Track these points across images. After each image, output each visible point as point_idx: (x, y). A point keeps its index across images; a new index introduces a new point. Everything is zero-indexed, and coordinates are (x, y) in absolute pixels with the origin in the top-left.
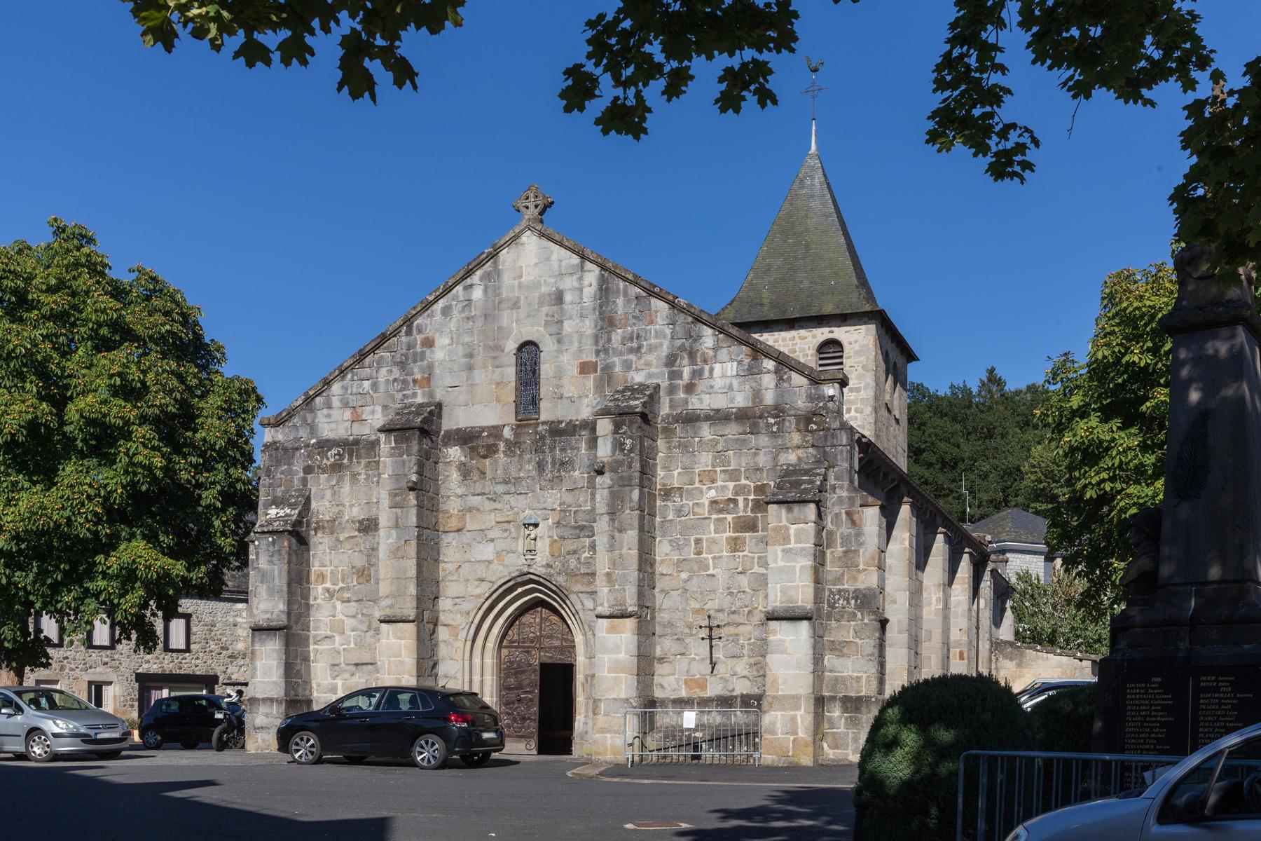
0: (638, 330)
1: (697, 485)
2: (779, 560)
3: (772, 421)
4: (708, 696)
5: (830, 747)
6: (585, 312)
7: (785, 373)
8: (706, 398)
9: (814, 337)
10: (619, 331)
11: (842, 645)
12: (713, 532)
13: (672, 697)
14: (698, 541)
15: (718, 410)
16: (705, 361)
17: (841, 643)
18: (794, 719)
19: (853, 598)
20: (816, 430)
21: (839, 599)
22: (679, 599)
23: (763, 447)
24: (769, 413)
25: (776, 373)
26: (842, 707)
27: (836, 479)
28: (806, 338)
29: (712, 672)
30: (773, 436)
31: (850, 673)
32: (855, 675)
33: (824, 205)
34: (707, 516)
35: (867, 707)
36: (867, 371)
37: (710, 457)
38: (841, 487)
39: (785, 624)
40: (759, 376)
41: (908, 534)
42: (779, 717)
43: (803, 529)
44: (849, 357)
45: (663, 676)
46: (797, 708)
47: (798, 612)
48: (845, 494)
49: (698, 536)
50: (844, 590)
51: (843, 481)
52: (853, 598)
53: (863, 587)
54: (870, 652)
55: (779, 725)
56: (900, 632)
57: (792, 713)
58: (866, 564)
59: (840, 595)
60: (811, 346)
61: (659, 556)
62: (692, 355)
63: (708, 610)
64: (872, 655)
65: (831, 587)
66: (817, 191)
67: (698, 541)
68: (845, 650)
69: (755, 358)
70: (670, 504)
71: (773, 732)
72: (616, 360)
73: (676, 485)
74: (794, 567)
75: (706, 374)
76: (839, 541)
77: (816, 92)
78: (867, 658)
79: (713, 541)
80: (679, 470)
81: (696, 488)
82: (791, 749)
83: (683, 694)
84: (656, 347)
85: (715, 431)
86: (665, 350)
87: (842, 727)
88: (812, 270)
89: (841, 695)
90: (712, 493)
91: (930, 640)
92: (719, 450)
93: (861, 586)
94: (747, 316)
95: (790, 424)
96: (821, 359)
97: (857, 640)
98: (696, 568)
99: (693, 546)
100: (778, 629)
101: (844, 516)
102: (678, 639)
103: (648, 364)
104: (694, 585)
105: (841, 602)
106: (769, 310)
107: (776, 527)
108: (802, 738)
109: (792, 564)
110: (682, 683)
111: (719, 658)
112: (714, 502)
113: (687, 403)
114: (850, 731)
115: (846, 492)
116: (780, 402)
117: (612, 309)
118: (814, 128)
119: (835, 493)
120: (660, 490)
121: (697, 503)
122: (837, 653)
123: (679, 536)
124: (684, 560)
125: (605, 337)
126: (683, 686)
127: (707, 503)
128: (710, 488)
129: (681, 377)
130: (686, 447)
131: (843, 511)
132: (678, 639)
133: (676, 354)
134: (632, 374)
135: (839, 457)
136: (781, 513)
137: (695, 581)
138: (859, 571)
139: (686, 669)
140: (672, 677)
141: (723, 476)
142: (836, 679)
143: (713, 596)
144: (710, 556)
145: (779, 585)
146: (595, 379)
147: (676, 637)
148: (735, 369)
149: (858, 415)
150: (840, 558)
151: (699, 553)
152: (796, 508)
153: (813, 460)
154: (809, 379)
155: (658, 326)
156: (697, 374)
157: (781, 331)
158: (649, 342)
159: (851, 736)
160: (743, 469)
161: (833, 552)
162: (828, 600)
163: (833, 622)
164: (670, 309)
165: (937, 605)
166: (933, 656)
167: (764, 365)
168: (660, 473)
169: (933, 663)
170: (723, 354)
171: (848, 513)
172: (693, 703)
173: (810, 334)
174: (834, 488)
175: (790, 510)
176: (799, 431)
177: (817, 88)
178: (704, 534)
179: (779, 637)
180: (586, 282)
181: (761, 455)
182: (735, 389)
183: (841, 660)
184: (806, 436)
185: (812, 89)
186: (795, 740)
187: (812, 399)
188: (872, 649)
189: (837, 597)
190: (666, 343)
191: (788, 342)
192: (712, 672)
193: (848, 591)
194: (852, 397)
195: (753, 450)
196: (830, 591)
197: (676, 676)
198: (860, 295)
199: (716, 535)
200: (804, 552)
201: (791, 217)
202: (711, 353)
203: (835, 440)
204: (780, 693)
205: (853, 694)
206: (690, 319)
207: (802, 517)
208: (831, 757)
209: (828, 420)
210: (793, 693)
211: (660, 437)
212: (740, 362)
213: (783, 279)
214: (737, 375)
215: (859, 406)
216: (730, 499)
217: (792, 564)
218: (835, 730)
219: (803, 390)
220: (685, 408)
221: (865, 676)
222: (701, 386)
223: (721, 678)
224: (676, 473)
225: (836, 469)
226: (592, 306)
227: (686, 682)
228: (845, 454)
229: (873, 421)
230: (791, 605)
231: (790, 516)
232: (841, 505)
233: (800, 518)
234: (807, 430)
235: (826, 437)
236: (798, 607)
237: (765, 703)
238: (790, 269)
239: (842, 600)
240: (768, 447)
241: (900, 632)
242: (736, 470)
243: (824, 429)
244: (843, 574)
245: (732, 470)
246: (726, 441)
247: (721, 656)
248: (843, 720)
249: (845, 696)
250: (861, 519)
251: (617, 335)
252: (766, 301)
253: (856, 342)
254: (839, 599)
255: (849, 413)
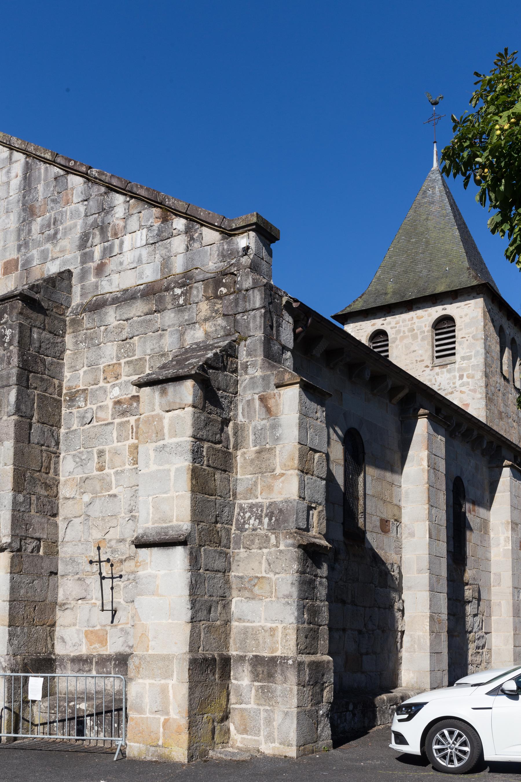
0: (55, 214)
1: (102, 384)
2: (151, 462)
3: (178, 291)
4: (108, 653)
5: (239, 732)
6: (10, 206)
7: (196, 231)
8: (115, 277)
9: (429, 315)
10: (39, 220)
11: (253, 583)
12: (115, 441)
13: (72, 654)
14: (101, 453)
15: (126, 290)
16: (115, 235)
17: (251, 579)
18: (164, 691)
19: (266, 515)
20: (226, 295)
21: (250, 518)
22: (80, 528)
23: (169, 326)
24: (176, 282)
25: (186, 233)
26: (252, 672)
27: (249, 354)
28: (422, 317)
29: (112, 622)
30: (179, 311)
31: (263, 623)
32: (269, 625)
33: (442, 208)
34: (110, 421)
35: (283, 672)
36: (477, 340)
37: (115, 348)
38: (254, 365)
39: (155, 551)
40: (169, 240)
41: (426, 453)
42: (147, 687)
43: (178, 416)
44: (461, 330)
45: (64, 627)
46: (168, 675)
47: (172, 534)
48: (259, 374)
49: (101, 447)
50: (257, 505)
51: (255, 356)
52: (266, 515)
53: (279, 499)
54: (286, 593)
55: (147, 700)
56: (420, 571)
57: (163, 682)
58: (284, 466)
59: (251, 512)
60: (427, 323)
61: (63, 477)
62: (103, 230)
63: (110, 540)
64: (289, 596)
65: (242, 501)
66: (437, 198)
67: (101, 453)
68: (256, 590)
69: (165, 220)
70: (74, 410)
71: (140, 710)
72: (35, 253)
73: (82, 387)
74: (169, 470)
75: (116, 250)
76: (251, 437)
77: (436, 120)
78: (283, 601)
79: (116, 453)
80: (85, 368)
81: (101, 388)
82: (161, 735)
83: (84, 650)
84: (71, 230)
85: (120, 315)
86: (78, 231)
87: (252, 702)
88: (431, 260)
89: (250, 655)
90: (116, 392)
91: (499, 584)
92: (124, 337)
93: (277, 498)
94: (373, 304)
95: (198, 292)
96: (437, 335)
97: (271, 575)
98: (98, 488)
99: (96, 460)
100: (148, 561)
101: (257, 403)
102: (79, 579)
103: (62, 251)
104: (95, 511)
105: (252, 521)
106: (391, 297)
107: (148, 417)
108: (174, 719)
109: (167, 467)
110: (82, 636)
111: (119, 602)
112: (118, 403)
113: (97, 287)
114: (262, 708)
115: (259, 370)
116: (190, 268)
117: (33, 198)
118: (435, 149)
119: (246, 373)
120: (66, 394)
121: (100, 406)
122: (247, 594)
123: (82, 449)
124: (87, 478)
125: (26, 229)
126: (84, 640)
127: (111, 404)
128: (114, 386)
129: (92, 259)
130: (92, 339)
131: (256, 397)
132: (79, 579)
133: (89, 233)
134: (49, 264)
135: (251, 325)
136: (154, 398)
137: (98, 503)
138: (275, 477)
139: (86, 619)
140: (73, 629)
141: (127, 369)
142: (245, 631)
143: (114, 523)
144: (112, 471)
145: (150, 498)
146: (16, 277)
147: (78, 576)
148: (144, 238)
149: (470, 380)
150: (252, 461)
151: (101, 469)
152: (171, 388)
153: (222, 333)
154: (222, 232)
155: (73, 205)
156: (107, 252)
157: (401, 313)
158: (65, 225)
159: (263, 715)
160: (148, 357)
161: (244, 453)
162: (237, 520)
163: (242, 550)
164: (85, 183)
165: (505, 546)
166: (503, 603)
167: (174, 226)
168: (67, 374)
169: (503, 610)
170: (133, 223)
171: (262, 399)
172: (91, 663)
173: (426, 313)
174: (246, 367)
175: (164, 392)
176: (208, 299)
177: (438, 117)
178: (106, 443)
179: (149, 571)
180: (13, 174)
181: (167, 336)
182: (144, 262)
183: (252, 604)
184: (215, 304)
185: (433, 118)
186: (166, 721)
187: (224, 256)
188: (289, 586)
189: (248, 515)
190: (80, 222)
191: (407, 322)
192: (112, 622)
193: (261, 506)
194: (464, 365)
195: (160, 332)
196: (241, 508)
197: (77, 627)
198: (470, 274)
199: (120, 444)
200: (180, 449)
201: (415, 221)
202: (121, 223)
203: (247, 304)
204: (150, 652)
205: (266, 654)
206: (103, 189)
207: (178, 400)
208: (239, 744)
209: (239, 279)
210: (165, 652)
211: (68, 331)
212: (150, 228)
213: (406, 272)
214: (147, 244)
215: (470, 372)
216: (133, 397)
217: (167, 467)
218: (243, 706)
219: (215, 247)
220: (95, 294)
221: (280, 626)
222: (112, 265)
223: (122, 630)
224: (81, 372)
225: (248, 342)
226: (17, 198)
227: (86, 634)
228: (258, 319)
229: (483, 384)
230: (164, 525)
231: (164, 400)
232: (253, 388)
233: (174, 402)
234: (217, 297)
235: (236, 301)
236: (172, 527)
237: (132, 663)
238: (411, 262)
239: (253, 518)
240: (174, 325)
241: (420, 571)
242: (140, 359)
243: (234, 292)
244: (255, 484)
245: (136, 360)
246: (131, 326)
247: (122, 602)
248: (253, 691)
249: (256, 656)
250: (277, 405)
251: (36, 226)
252: (390, 291)
253: (466, 315)
254: (250, 518)
255: (462, 379)
